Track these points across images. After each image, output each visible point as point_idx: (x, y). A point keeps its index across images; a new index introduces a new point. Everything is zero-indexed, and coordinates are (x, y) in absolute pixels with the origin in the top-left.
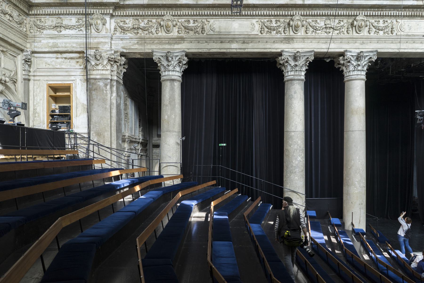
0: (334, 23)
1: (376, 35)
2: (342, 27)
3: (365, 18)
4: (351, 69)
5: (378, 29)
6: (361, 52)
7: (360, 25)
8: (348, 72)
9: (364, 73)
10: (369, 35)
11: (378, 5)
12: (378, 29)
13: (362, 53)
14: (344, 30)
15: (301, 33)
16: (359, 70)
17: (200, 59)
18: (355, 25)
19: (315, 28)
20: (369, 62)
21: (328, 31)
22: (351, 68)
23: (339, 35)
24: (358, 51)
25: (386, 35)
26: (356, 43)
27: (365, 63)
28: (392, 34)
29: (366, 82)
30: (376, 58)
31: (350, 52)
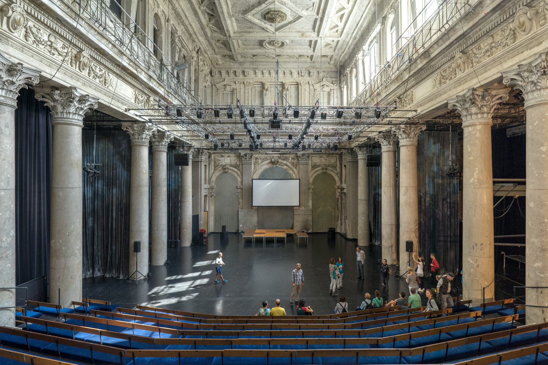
0: (59, 44)
4: (71, 111)
5: (38, 41)
8: (67, 113)
9: (81, 118)
12: (96, 76)
13: (87, 97)
15: (19, 34)
17: (420, 224)
19: (38, 39)
20: (89, 109)
21: (53, 51)
22: (72, 110)
24: (84, 93)
26: (78, 81)
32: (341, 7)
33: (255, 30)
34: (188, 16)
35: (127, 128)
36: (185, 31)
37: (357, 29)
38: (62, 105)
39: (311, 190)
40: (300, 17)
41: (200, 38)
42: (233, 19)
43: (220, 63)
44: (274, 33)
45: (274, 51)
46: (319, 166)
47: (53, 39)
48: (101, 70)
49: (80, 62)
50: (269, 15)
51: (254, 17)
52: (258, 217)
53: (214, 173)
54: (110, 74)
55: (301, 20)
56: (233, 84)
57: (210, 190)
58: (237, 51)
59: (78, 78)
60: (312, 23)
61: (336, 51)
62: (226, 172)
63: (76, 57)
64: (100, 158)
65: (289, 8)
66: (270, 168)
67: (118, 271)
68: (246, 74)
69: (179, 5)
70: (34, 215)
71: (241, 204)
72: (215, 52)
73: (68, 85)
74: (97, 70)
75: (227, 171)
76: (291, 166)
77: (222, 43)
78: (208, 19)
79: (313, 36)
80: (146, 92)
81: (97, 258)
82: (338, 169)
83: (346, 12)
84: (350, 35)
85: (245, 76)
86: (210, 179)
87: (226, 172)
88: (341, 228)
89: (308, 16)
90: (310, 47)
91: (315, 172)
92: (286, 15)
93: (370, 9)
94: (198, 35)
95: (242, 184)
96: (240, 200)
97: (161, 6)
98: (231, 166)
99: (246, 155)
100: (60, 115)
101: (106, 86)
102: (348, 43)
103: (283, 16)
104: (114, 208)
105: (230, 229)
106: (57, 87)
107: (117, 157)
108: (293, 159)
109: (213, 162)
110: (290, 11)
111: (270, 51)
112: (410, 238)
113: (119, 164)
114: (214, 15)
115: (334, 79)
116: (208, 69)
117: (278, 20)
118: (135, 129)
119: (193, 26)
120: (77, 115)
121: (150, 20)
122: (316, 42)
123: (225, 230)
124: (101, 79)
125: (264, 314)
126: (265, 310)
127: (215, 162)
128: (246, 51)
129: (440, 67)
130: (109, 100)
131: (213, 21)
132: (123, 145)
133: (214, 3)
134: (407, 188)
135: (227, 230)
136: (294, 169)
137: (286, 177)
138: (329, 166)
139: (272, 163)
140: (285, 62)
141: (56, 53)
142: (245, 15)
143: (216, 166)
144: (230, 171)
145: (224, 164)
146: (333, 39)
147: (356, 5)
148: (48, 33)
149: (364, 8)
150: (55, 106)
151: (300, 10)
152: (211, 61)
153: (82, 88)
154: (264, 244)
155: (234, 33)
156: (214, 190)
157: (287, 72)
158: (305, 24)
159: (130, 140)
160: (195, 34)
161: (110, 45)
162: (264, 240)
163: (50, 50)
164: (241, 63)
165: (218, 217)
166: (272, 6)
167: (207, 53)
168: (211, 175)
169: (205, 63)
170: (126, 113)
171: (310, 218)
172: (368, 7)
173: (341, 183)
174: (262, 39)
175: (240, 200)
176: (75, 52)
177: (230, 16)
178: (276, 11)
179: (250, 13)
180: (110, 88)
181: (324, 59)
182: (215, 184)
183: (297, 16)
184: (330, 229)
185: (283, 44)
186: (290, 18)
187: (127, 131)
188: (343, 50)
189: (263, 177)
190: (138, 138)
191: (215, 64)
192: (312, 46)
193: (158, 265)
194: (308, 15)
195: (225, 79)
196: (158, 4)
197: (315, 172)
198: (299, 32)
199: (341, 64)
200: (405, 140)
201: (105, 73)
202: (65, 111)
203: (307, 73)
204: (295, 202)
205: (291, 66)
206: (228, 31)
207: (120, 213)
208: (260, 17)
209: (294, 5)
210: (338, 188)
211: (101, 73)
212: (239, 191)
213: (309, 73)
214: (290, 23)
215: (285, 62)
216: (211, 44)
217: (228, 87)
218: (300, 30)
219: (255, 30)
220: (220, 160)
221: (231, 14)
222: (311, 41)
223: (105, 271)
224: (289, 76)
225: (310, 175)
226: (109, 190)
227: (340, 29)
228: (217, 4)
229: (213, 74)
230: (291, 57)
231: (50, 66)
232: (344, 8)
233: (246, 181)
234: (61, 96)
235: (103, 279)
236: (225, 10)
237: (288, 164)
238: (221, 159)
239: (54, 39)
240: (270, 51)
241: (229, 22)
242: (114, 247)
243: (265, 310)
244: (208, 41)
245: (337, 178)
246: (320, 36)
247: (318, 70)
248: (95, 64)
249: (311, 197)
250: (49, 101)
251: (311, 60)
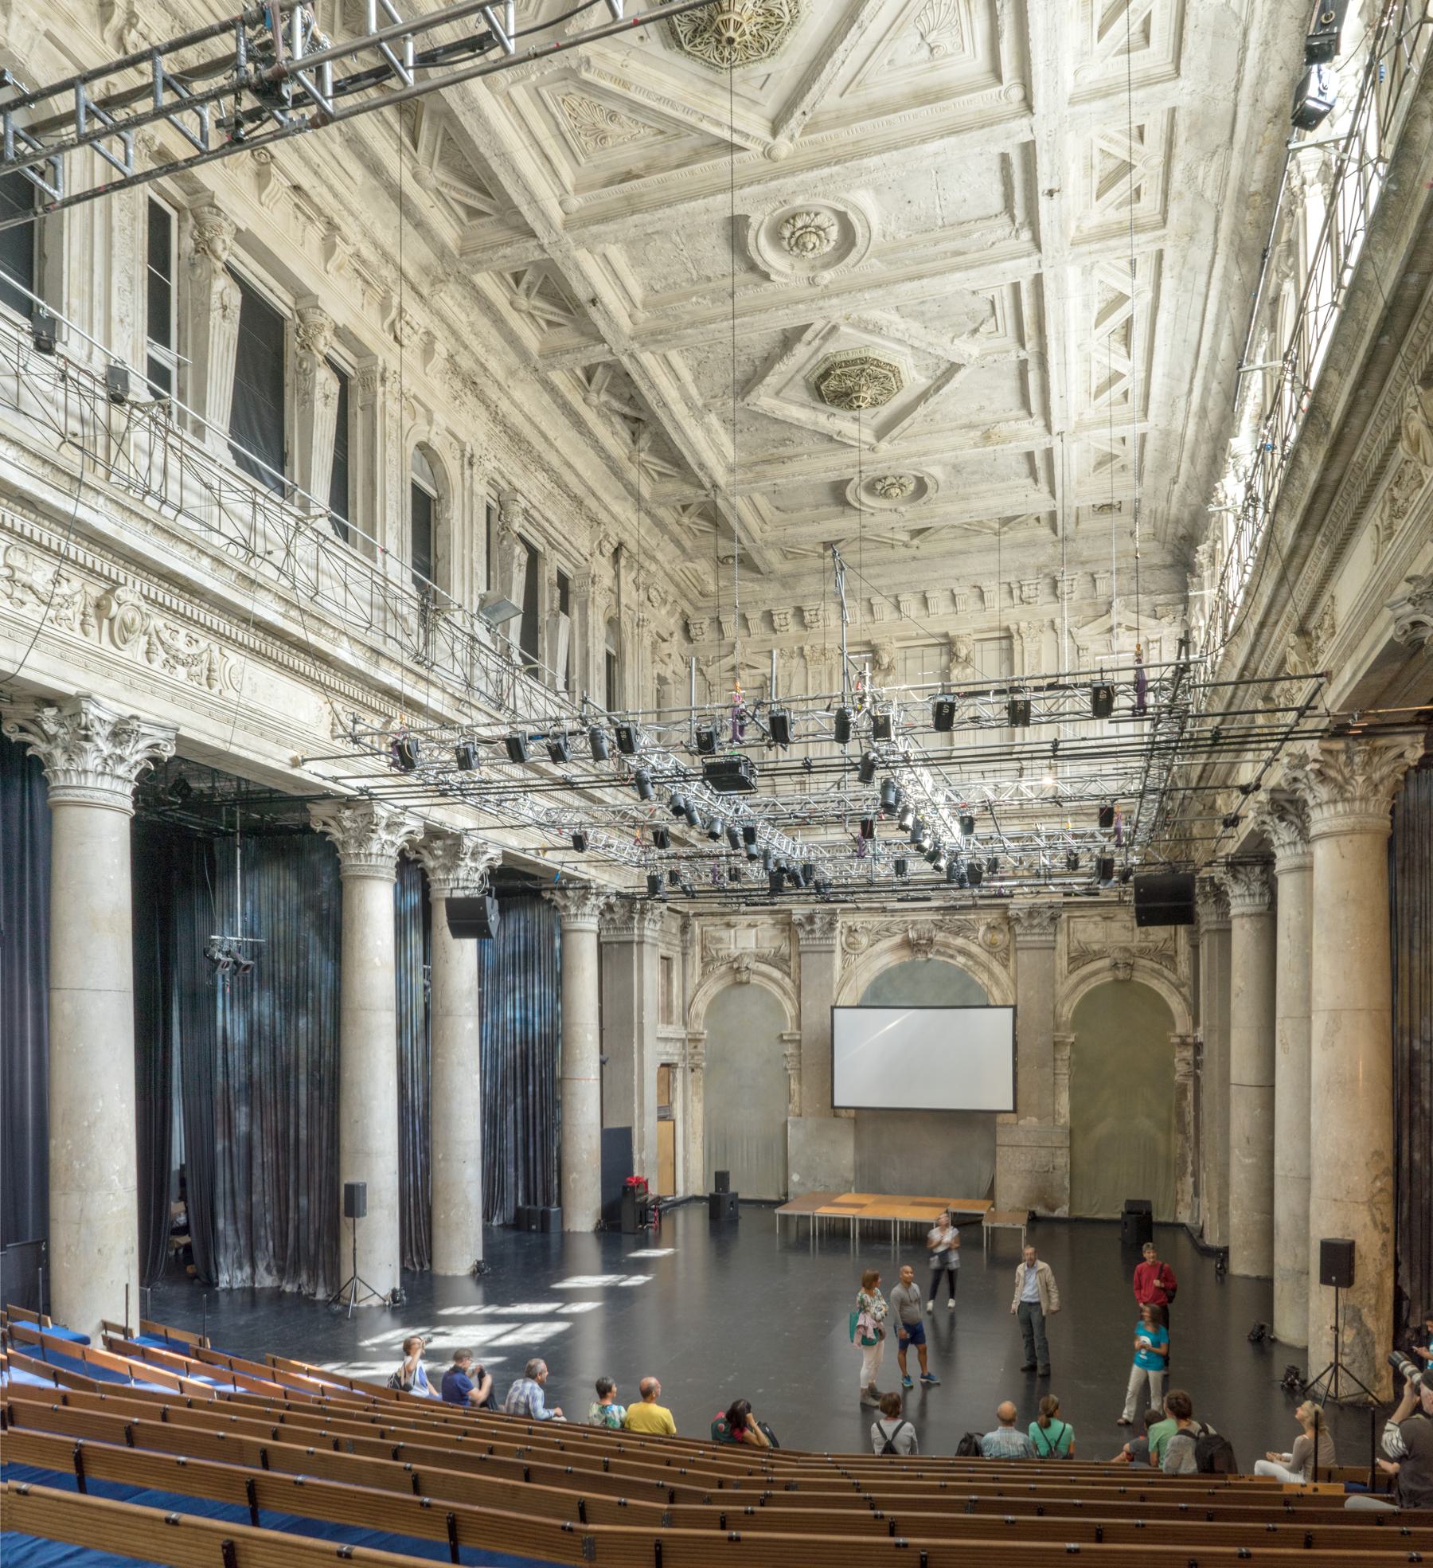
1: (166, 672)
2: (68, 601)
3: (144, 606)
4: (90, 766)
5: (174, 659)
6: (133, 717)
7: (128, 620)
8: (79, 773)
9: (128, 790)
10: (147, 664)
11: (187, 580)
12: (174, 659)
13: (135, 723)
14: (73, 613)
16: (119, 777)
18: (112, 614)
21: (17, 594)
22: (92, 762)
23: (56, 626)
24: (128, 712)
25: (195, 684)
26: (109, 676)
27: (138, 757)
28: (210, 687)
29: (135, 821)
30: (172, 754)
31: (98, 704)
32: (1111, 296)
33: (800, 449)
34: (551, 435)
35: (325, 824)
36: (556, 491)
37: (1200, 374)
38: (66, 750)
39: (1066, 1052)
40: (954, 368)
41: (616, 508)
42: (713, 419)
43: (712, 588)
44: (873, 449)
45: (894, 516)
46: (1098, 955)
47: (17, 559)
48: (191, 641)
49: (112, 620)
50: (833, 383)
51: (782, 400)
52: (858, 1147)
53: (700, 985)
54: (226, 652)
55: (960, 376)
56: (762, 660)
57: (689, 1049)
58: (757, 534)
59: (109, 667)
60: (1011, 384)
61: (1148, 479)
62: (741, 983)
63: (98, 606)
64: (264, 924)
65: (899, 341)
66: (902, 967)
67: (313, 1278)
68: (807, 617)
69: (513, 402)
70: (23, 1070)
71: (796, 1098)
72: (683, 550)
73: (72, 690)
74: (180, 642)
75: (744, 977)
76: (983, 956)
77: (701, 515)
78: (627, 436)
79: (1029, 434)
80: (375, 703)
81: (263, 1233)
82: (1184, 969)
83: (1138, 309)
84: (1182, 403)
85: (805, 627)
86: (687, 1009)
87: (741, 983)
88: (1195, 1208)
89: (983, 356)
90: (1036, 481)
91: (1084, 979)
92: (895, 371)
93: (1226, 277)
94: (607, 498)
95: (799, 1027)
96: (794, 1086)
97: (438, 417)
98: (761, 958)
99: (810, 919)
100: (62, 778)
101: (215, 691)
102: (1183, 436)
103: (884, 377)
104: (303, 1077)
105: (742, 1187)
106: (49, 699)
107: (309, 917)
108: (991, 928)
109: (698, 948)
110: (908, 351)
111: (879, 518)
112: (1346, 1227)
113: (313, 939)
114: (642, 417)
115: (1161, 599)
116: (670, 614)
117: (867, 394)
118: (347, 824)
119: (580, 466)
120: (108, 779)
121: (389, 469)
122: (1049, 454)
123: (726, 1189)
124: (194, 669)
125: (598, 1422)
126: (603, 1409)
127: (704, 948)
128: (791, 530)
129: (1382, 468)
130: (226, 731)
131: (645, 441)
132: (325, 879)
133: (627, 374)
134: (1336, 1013)
135: (732, 1189)
136: (997, 968)
137: (970, 999)
138: (1143, 952)
139: (909, 945)
140: (951, 554)
141: (30, 598)
142: (748, 399)
143: (707, 962)
144: (755, 980)
145: (735, 952)
146: (1118, 432)
147: (1166, 273)
148: (4, 544)
149: (1202, 279)
150: (50, 754)
151: (946, 339)
152: (677, 585)
153: (124, 696)
154: (855, 1244)
155: (731, 470)
156: (701, 1048)
157: (964, 591)
158: (982, 389)
159: (339, 862)
160: (594, 494)
161: (206, 562)
162: (856, 1230)
163: (9, 591)
164: (787, 581)
165: (717, 1141)
166: (831, 348)
167: (653, 559)
168: (690, 993)
169: (653, 594)
170: (296, 772)
171: (1062, 1160)
172: (1218, 271)
173: (1196, 1023)
174: (834, 476)
175: (794, 1086)
176: (95, 590)
177: (699, 413)
178: (854, 362)
179: (761, 389)
180: (230, 694)
181: (1106, 521)
182: (706, 1026)
183: (944, 366)
184: (1129, 1203)
185: (921, 487)
186: (914, 379)
187: (325, 834)
188: (1172, 474)
189: (877, 998)
190: (357, 855)
191: (694, 594)
192: (1042, 474)
193: (450, 1273)
194: (986, 353)
195: (733, 646)
196: (428, 411)
197: (1084, 979)
198: (971, 426)
199: (1181, 531)
200: (1328, 811)
201: (209, 649)
202: (74, 766)
203: (1044, 586)
204: (996, 1095)
205: (979, 565)
206: (702, 466)
207: (316, 1093)
208: (805, 396)
209: (915, 327)
210: (1184, 1043)
211: (194, 650)
212: (790, 1049)
213: (1055, 584)
214: (924, 397)
215: (951, 554)
216: (659, 523)
217: (745, 674)
218: (975, 418)
219: (800, 449)
220: (720, 940)
221: (700, 403)
222: (1030, 456)
223: (282, 1272)
224: (973, 604)
225: (1062, 989)
226: (288, 1020)
227: (1133, 382)
228: (635, 376)
229: (693, 632)
230: (970, 530)
231: (10, 637)
232: (1122, 299)
233: (814, 1016)
234: (62, 725)
235: (278, 1294)
236: (671, 393)
237: (974, 949)
238: (724, 934)
239: (23, 559)
240: (879, 518)
241: (696, 434)
242: (303, 1201)
243: (603, 1409)
244: (648, 513)
245: (1176, 1004)
246: (1056, 428)
247: (1089, 568)
248: (172, 625)
249: (1064, 1080)
250: (38, 742)
251: (1055, 530)
